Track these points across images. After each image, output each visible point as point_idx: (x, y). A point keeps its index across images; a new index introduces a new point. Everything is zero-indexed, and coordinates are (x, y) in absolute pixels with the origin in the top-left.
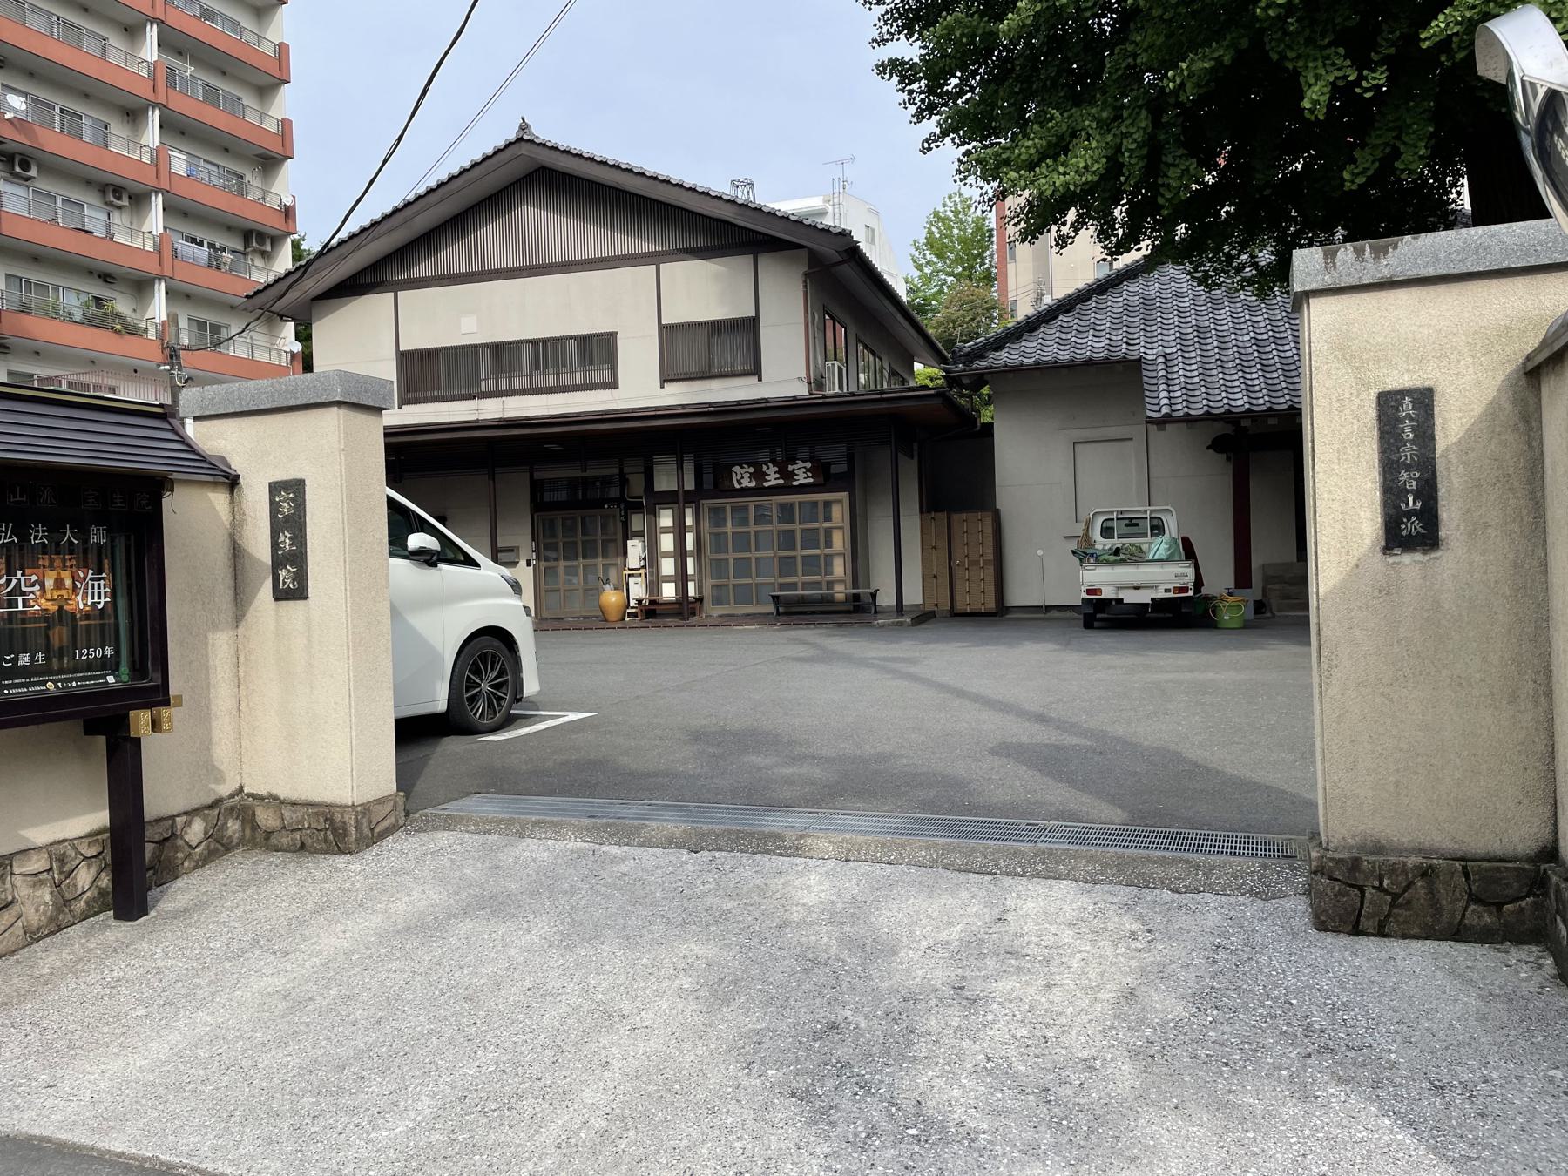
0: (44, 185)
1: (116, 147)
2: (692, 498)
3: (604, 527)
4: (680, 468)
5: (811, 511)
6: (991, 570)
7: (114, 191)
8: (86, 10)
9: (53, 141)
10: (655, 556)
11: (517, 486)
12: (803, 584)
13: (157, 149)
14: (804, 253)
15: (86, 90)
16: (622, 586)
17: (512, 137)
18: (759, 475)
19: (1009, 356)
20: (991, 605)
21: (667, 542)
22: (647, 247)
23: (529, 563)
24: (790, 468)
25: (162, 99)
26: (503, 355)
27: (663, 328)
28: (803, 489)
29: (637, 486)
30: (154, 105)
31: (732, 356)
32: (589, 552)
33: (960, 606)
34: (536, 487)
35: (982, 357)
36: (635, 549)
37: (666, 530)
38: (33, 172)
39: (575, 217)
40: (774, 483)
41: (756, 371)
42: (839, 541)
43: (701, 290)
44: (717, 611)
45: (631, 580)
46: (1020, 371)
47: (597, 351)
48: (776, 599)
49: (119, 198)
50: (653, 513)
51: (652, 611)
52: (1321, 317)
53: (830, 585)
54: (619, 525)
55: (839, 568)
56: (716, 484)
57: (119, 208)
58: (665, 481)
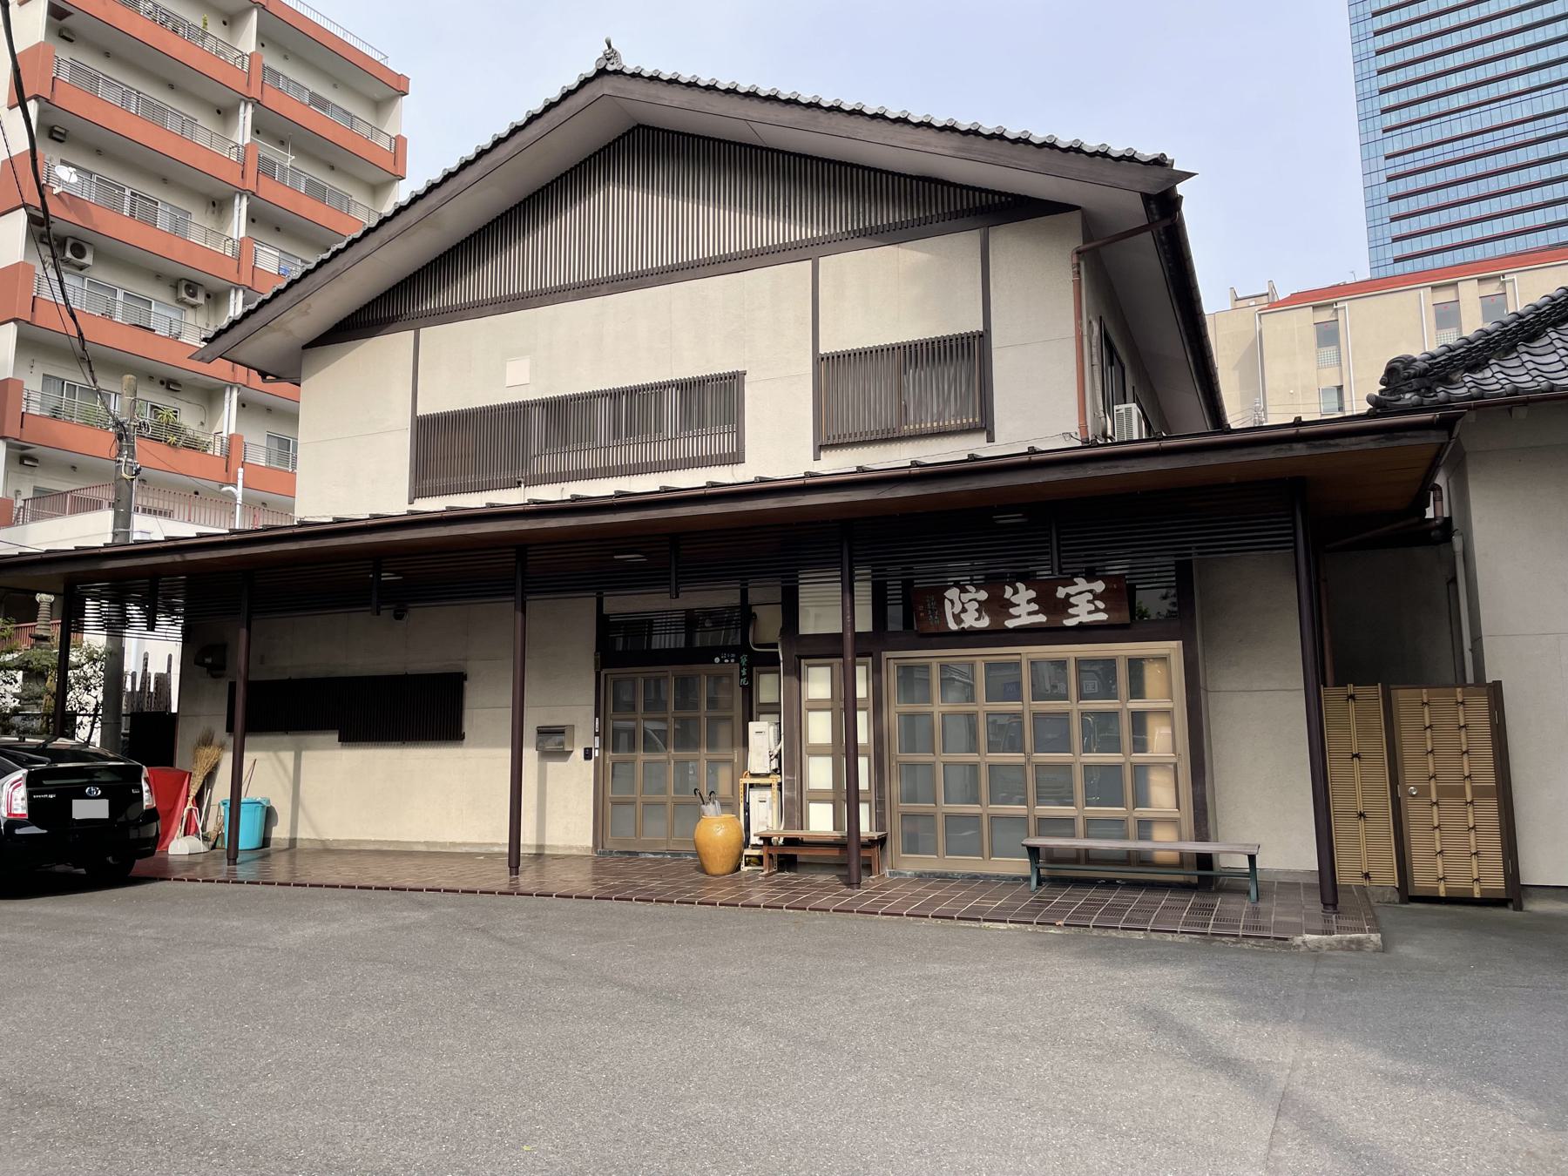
0: (101, 275)
1: (196, 237)
2: (869, 646)
3: (712, 703)
4: (849, 590)
5: (1102, 676)
6: (1490, 809)
7: (188, 287)
8: (171, 87)
9: (117, 225)
10: (792, 759)
11: (570, 625)
12: (1089, 822)
13: (241, 241)
14: (1075, 217)
15: (165, 173)
16: (737, 805)
17: (590, 70)
18: (997, 606)
19: (1494, 378)
20: (1496, 882)
21: (819, 728)
22: (798, 232)
23: (588, 755)
24: (1061, 592)
25: (250, 185)
26: (563, 414)
27: (820, 360)
28: (1085, 633)
29: (768, 625)
30: (242, 192)
31: (937, 395)
32: (686, 739)
33: (1422, 880)
34: (605, 626)
35: (1446, 381)
36: (763, 737)
37: (817, 706)
38: (88, 260)
39: (685, 196)
40: (1025, 620)
41: (985, 426)
42: (1163, 739)
43: (889, 293)
44: (911, 865)
45: (754, 796)
46: (1517, 401)
47: (714, 400)
48: (1033, 852)
49: (194, 295)
50: (796, 673)
51: (788, 856)
52: (304, 833)
53: (1145, 827)
54: (738, 693)
55: (1162, 795)
56: (907, 623)
57: (194, 306)
58: (820, 612)
